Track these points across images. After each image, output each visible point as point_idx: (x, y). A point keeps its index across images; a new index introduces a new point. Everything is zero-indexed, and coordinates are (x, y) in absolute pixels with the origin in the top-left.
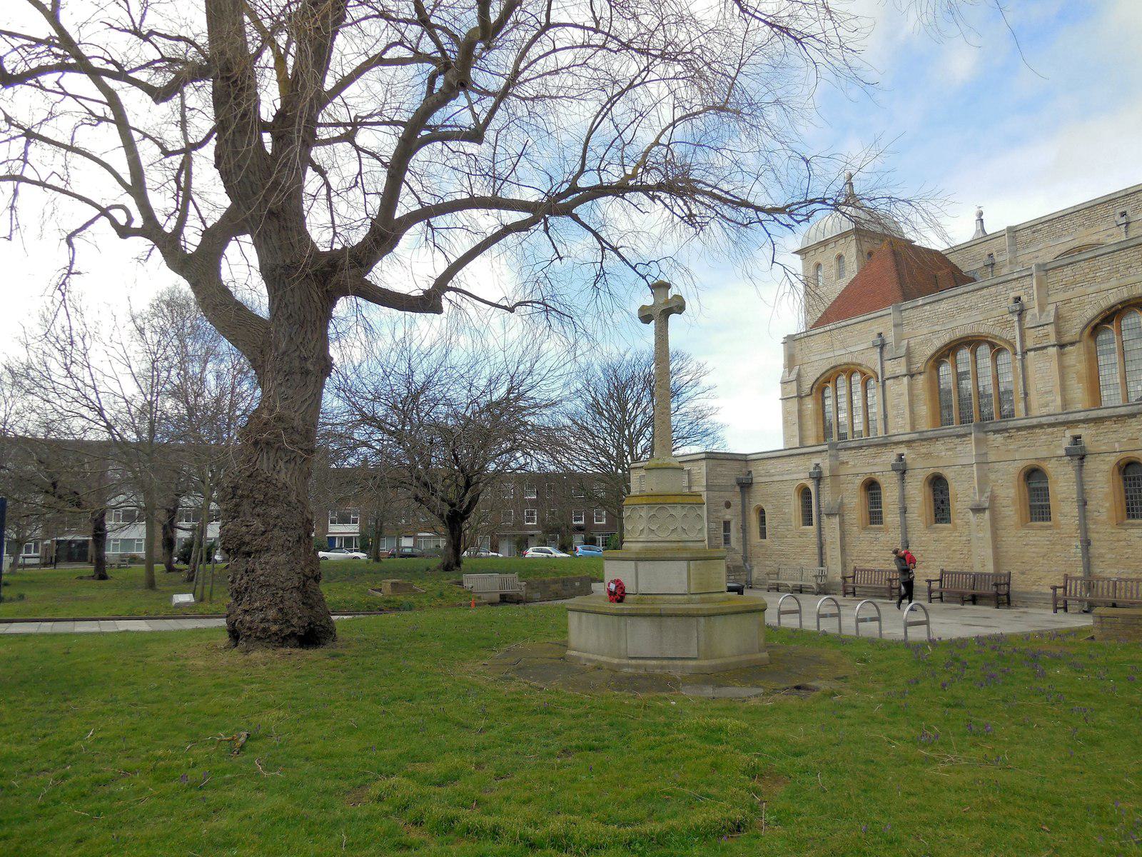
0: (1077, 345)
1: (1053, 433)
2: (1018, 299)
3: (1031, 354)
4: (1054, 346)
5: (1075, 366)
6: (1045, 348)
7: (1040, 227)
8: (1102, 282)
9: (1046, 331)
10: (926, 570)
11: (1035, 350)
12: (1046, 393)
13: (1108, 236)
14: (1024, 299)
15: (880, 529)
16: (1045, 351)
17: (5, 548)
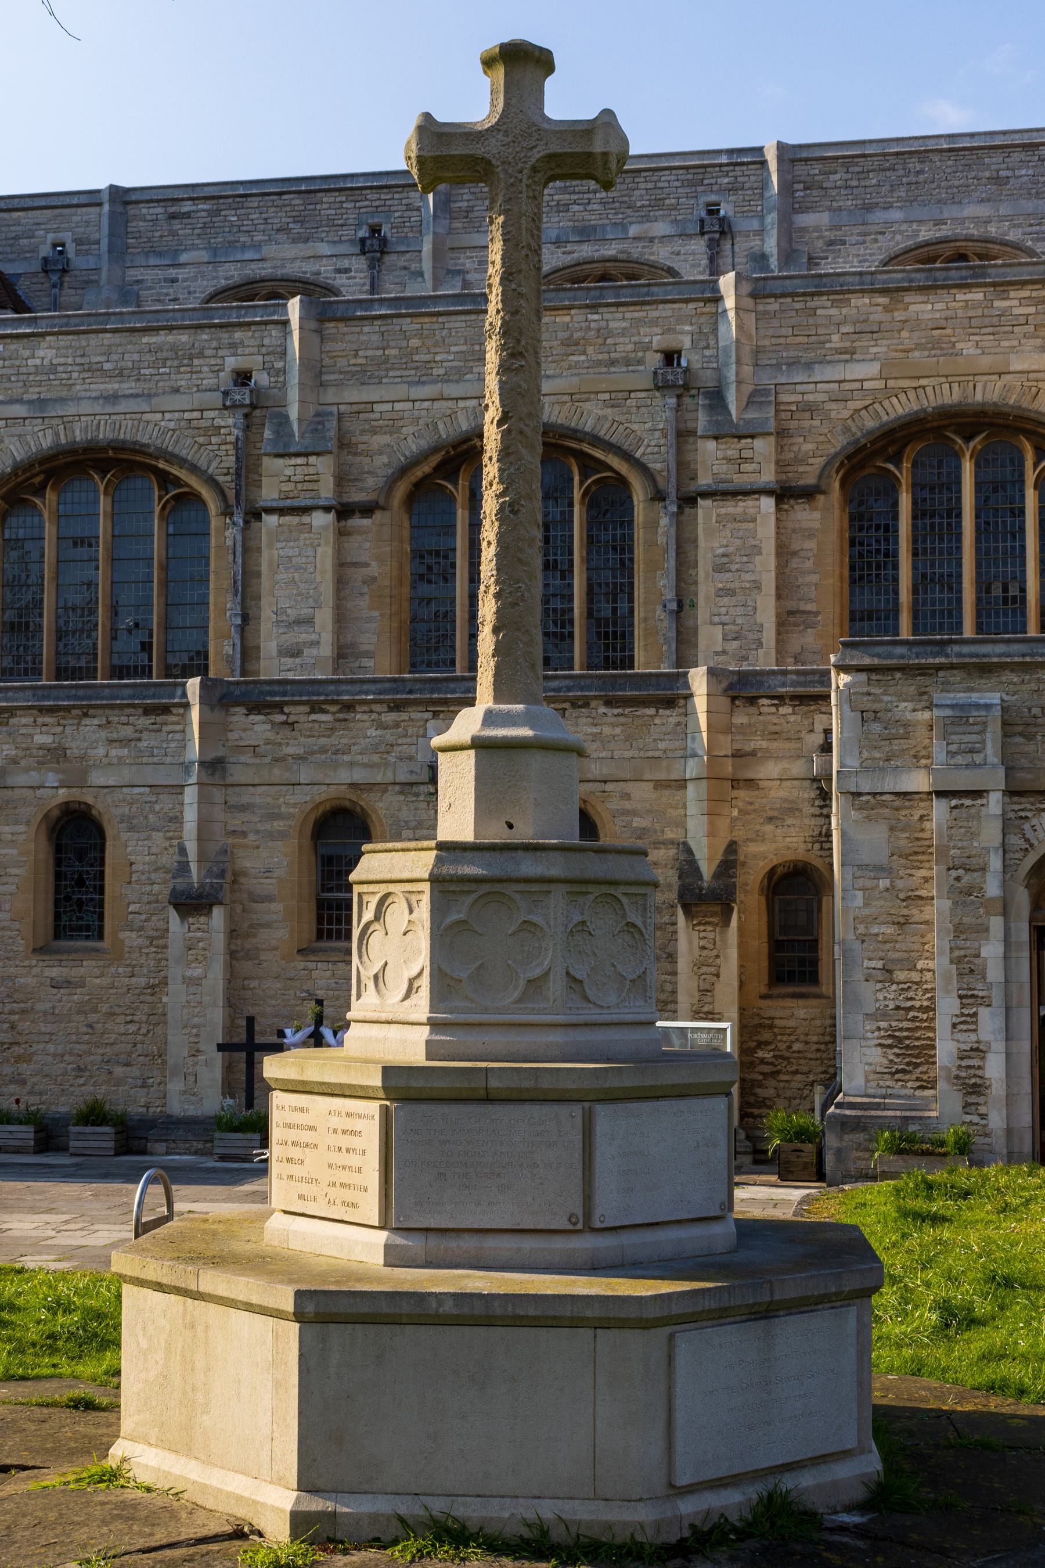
0: (378, 515)
1: (397, 725)
2: (243, 377)
3: (271, 521)
4: (327, 509)
5: (366, 565)
6: (306, 510)
7: (187, 207)
8: (445, 379)
9: (312, 470)
10: (24, 1067)
11: (282, 511)
12: (298, 622)
13: (339, 271)
14: (261, 378)
15: (96, 950)
16: (306, 519)
17: (443, 1038)
